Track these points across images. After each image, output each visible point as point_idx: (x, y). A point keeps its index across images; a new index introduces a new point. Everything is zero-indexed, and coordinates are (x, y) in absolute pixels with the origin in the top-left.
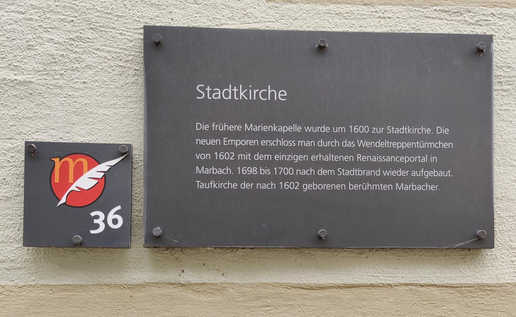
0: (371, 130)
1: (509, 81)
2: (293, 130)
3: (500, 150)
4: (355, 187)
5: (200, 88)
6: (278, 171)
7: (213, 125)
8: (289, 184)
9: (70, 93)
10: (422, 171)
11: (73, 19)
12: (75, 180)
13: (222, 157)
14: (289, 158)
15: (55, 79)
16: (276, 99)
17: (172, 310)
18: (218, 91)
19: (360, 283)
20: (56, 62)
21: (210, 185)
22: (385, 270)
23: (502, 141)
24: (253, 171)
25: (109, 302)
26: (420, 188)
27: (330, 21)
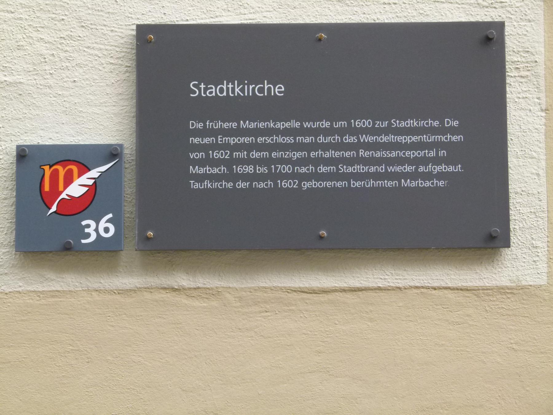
0: (374, 124)
1: (527, 67)
2: (291, 126)
3: (519, 141)
4: (358, 184)
5: (194, 85)
6: (276, 168)
7: (208, 123)
8: (287, 182)
9: (60, 93)
10: (430, 166)
11: (64, 18)
12: (65, 187)
13: (216, 156)
14: (287, 155)
15: (45, 79)
16: (273, 94)
17: (164, 316)
18: (212, 88)
19: (367, 286)
20: (46, 62)
21: (204, 185)
22: (393, 272)
23: (521, 132)
24: (249, 169)
25: (98, 308)
26: (428, 184)
27: (331, 8)
